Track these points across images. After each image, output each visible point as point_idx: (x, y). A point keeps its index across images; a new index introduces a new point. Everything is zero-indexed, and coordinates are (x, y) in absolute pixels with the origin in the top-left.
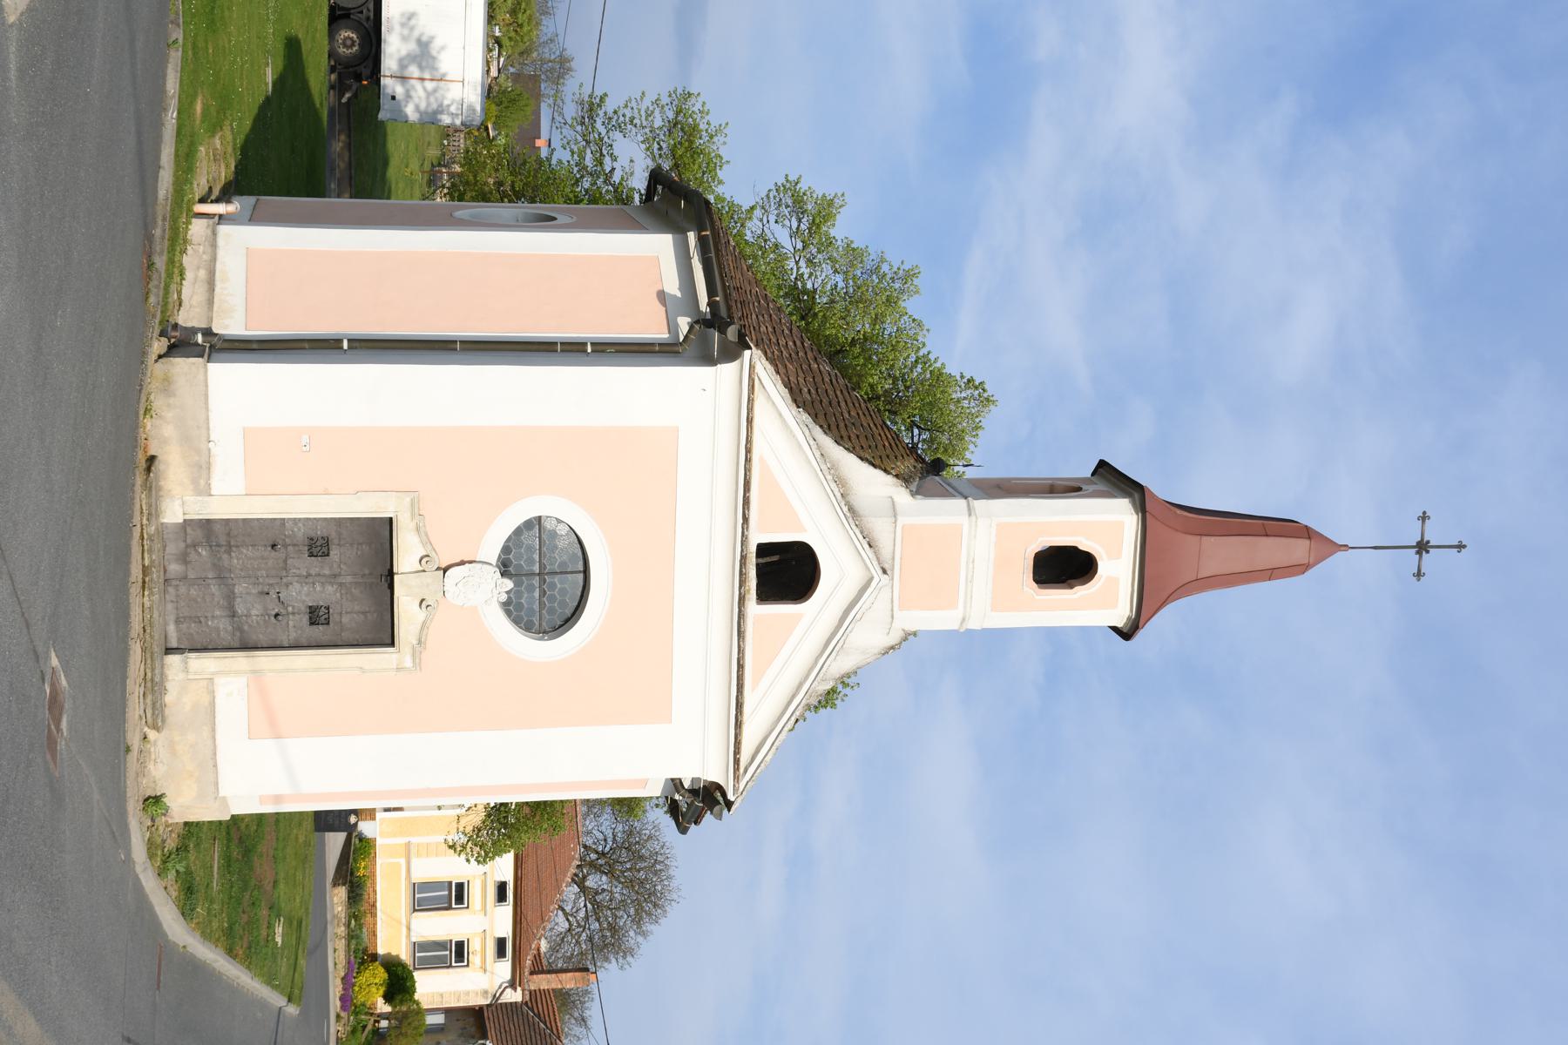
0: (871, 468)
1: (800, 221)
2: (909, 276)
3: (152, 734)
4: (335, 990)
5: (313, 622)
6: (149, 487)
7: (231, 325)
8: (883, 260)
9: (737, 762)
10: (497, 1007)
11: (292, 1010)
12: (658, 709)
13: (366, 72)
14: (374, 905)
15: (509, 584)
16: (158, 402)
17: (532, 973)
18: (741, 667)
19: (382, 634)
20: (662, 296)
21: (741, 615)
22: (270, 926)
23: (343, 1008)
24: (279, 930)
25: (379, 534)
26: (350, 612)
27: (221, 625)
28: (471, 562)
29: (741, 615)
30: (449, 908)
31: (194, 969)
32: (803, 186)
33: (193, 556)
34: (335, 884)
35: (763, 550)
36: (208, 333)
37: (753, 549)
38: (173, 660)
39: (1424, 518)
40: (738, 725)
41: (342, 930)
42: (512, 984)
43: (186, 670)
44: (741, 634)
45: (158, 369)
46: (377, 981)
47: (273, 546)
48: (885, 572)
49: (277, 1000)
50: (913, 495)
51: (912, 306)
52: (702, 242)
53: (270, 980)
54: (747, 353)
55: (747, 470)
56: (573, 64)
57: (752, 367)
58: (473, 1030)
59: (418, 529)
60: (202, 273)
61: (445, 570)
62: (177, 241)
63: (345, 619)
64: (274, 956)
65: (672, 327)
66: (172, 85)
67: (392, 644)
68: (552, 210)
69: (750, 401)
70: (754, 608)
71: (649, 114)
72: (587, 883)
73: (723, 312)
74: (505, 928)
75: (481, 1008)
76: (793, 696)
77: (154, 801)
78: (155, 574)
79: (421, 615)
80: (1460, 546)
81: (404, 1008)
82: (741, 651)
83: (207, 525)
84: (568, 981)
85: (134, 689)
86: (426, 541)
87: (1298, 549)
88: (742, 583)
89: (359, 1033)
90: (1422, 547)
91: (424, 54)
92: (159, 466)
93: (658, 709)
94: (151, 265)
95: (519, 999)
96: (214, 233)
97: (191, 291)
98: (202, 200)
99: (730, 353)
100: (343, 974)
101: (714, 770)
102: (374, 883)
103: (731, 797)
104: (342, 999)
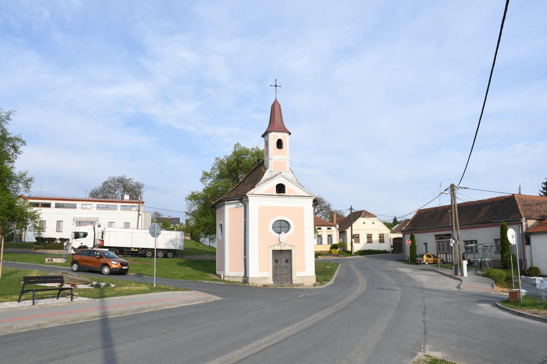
0: (264, 175)
1: (207, 178)
2: (217, 158)
3: (304, 285)
4: (336, 258)
5: (288, 262)
6: (268, 286)
7: (242, 274)
8: (214, 163)
9: (310, 197)
10: (339, 229)
11: (340, 265)
12: (301, 209)
13: (175, 252)
14: (321, 251)
15: (282, 232)
16: (255, 285)
17: (333, 223)
18: (295, 196)
19: (290, 252)
20: (236, 208)
21: (288, 196)
22: (328, 269)
23: (339, 256)
24: (328, 267)
25: (275, 252)
26: (286, 256)
27: (288, 275)
28: (279, 238)
29: (288, 196)
30: (322, 238)
31: (336, 280)
32: (201, 178)
33: (278, 280)
34: (318, 258)
35: (277, 193)
36: (244, 277)
37: (277, 194)
38: (293, 282)
39: (271, 86)
40: (304, 196)
41: (325, 257)
42: (336, 226)
43: (295, 281)
44: (291, 196)
45: (250, 284)
46: (334, 251)
47: (276, 268)
48: (281, 173)
49: (339, 267)
50: (268, 168)
51: (222, 158)
52: (227, 201)
53: (336, 268)
54: (247, 195)
55: (265, 195)
56: (156, 212)
57: (249, 194)
58: (343, 234)
59: (274, 246)
60: (234, 278)
61: (280, 242)
62: (229, 282)
63: (287, 257)
64: (332, 268)
65: (241, 206)
66: (207, 282)
67: (291, 250)
68: (218, 224)
69: (255, 194)
70: (286, 194)
71: (189, 205)
72: (316, 212)
73: (240, 198)
74: (326, 228)
75: (339, 232)
76: (300, 188)
77: (314, 285)
78: (281, 285)
79: (287, 246)
80: (276, 80)
81: (339, 246)
82: (293, 196)
83: (273, 277)
84: (335, 216)
85: (299, 287)
86: (276, 245)
87: (276, 106)
88: (282, 196)
89: (343, 254)
90: (276, 86)
91: (172, 241)
92: (265, 284)
93: (301, 209)
94: (236, 285)
95: (338, 225)
96: (227, 276)
97: (237, 280)
98: (221, 278)
99: (247, 197)
100: (333, 257)
101: (311, 200)
102: (317, 251)
103: (315, 198)
104: (337, 257)
